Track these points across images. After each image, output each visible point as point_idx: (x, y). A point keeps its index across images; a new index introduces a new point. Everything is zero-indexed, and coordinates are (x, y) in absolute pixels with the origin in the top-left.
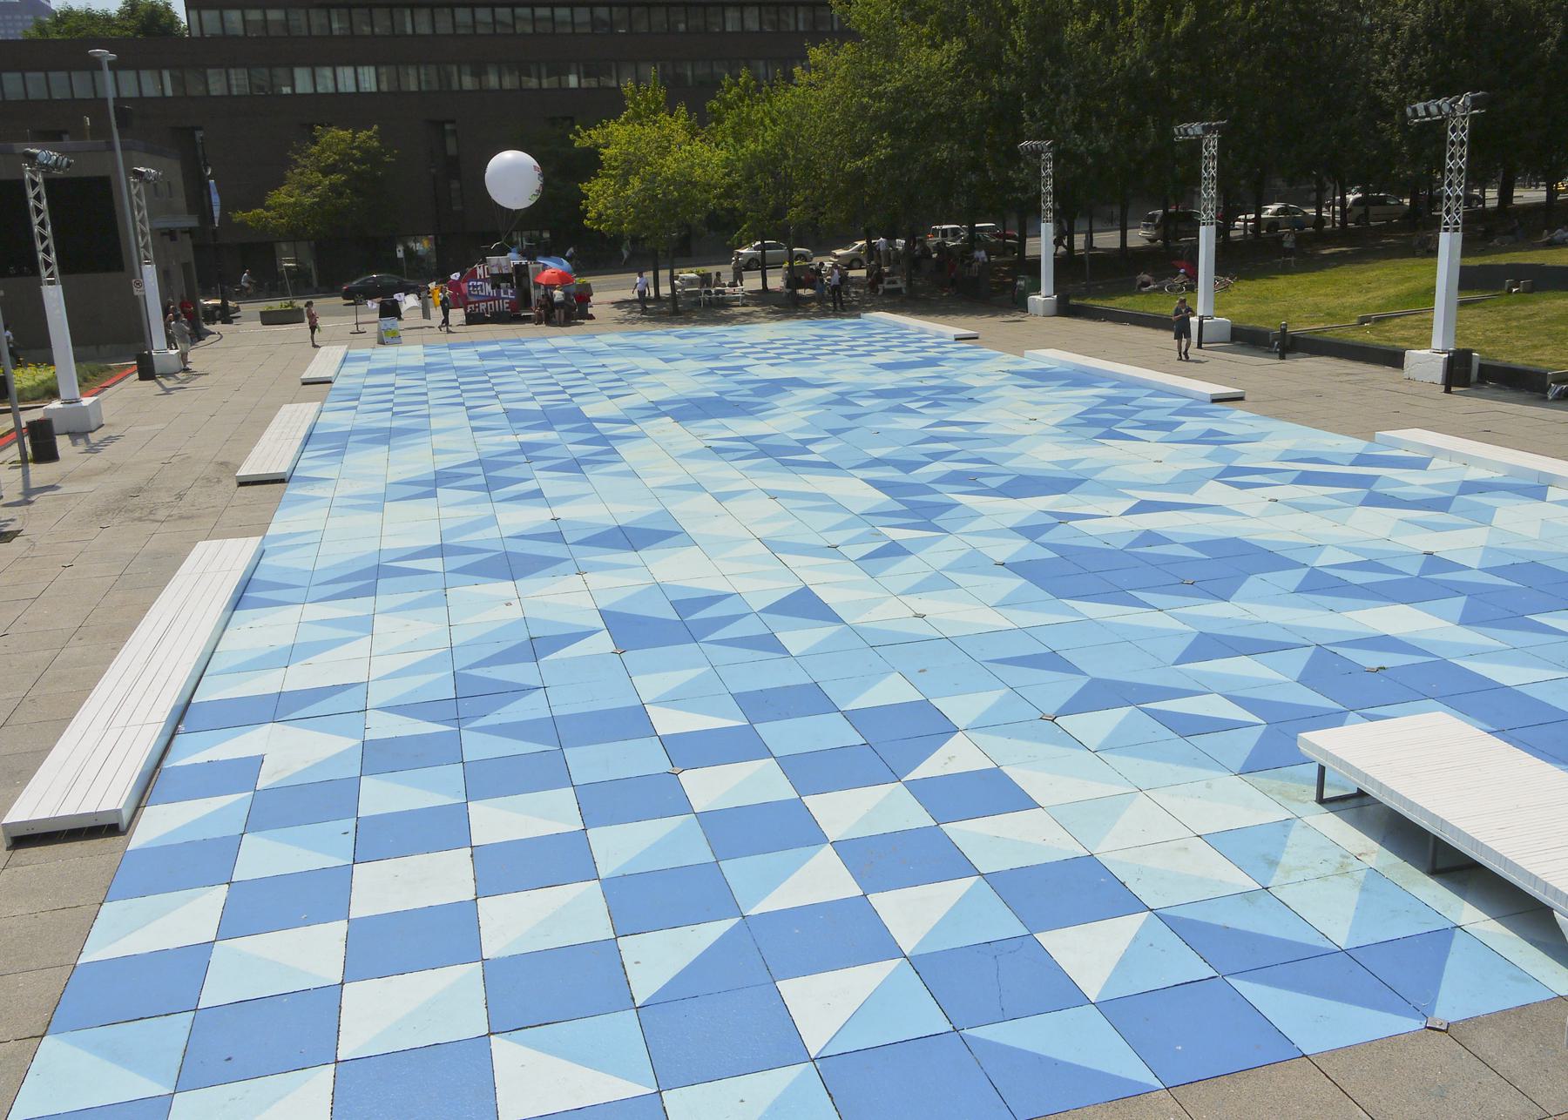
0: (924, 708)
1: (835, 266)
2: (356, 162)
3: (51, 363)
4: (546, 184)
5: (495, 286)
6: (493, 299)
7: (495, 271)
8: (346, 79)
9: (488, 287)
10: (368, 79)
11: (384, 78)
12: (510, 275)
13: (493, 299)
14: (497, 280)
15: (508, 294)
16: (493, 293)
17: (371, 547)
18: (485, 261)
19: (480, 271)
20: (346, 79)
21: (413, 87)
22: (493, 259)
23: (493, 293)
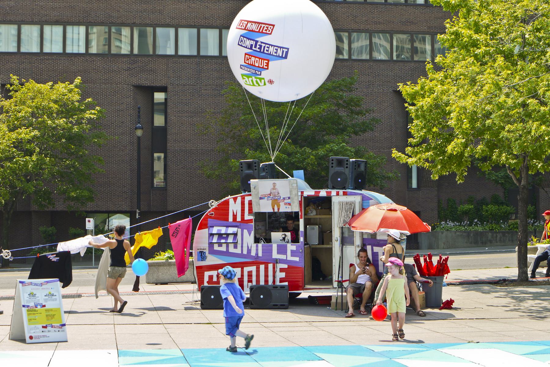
0: (133, 245)
1: (482, 209)
2: (50, 116)
3: (250, 192)
4: (316, 98)
5: (263, 237)
6: (256, 262)
7: (266, 207)
8: (54, 40)
9: (249, 238)
10: (77, 39)
11: (94, 38)
12: (294, 217)
13: (256, 262)
14: (268, 224)
15: (286, 252)
16: (258, 250)
17: (76, 292)
18: (247, 188)
19: (234, 207)
20: (54, 40)
21: (125, 50)
22: (261, 186)
23: (258, 250)
